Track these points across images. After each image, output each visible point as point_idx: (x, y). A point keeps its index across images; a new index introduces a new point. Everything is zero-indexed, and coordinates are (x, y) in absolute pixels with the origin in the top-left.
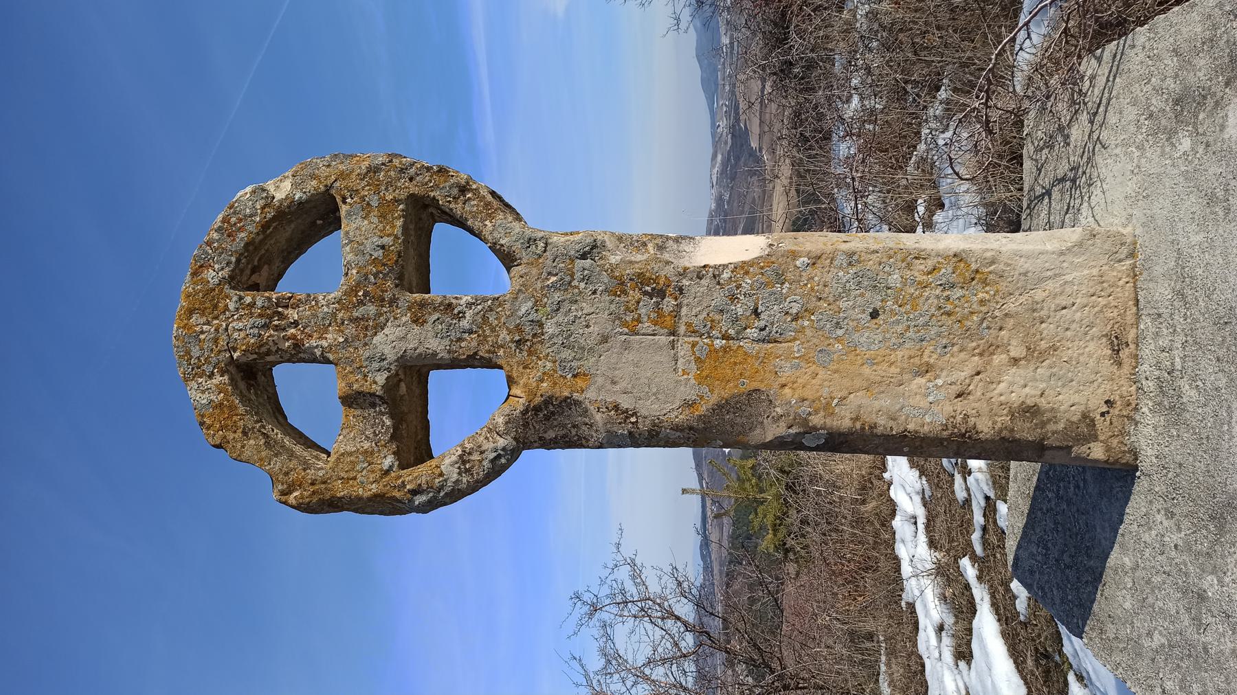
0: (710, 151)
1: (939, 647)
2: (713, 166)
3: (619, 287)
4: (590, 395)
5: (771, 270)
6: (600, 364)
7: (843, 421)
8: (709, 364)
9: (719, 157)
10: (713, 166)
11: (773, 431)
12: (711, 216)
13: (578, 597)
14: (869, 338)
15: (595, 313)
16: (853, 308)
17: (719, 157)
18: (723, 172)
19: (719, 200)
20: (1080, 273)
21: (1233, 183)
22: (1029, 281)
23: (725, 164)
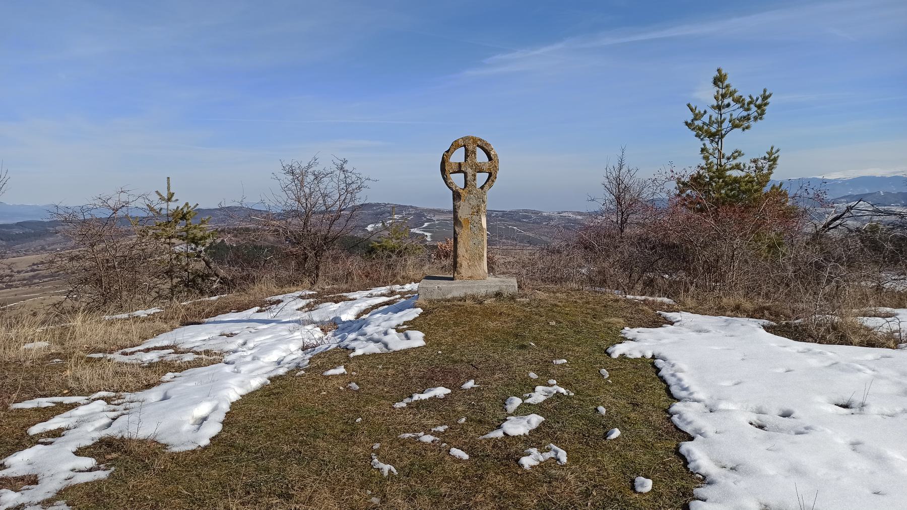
0: (584, 211)
1: (292, 322)
2: (574, 213)
3: (478, 206)
4: (461, 202)
5: (481, 229)
6: (466, 203)
7: (459, 240)
8: (467, 220)
9: (580, 217)
10: (574, 213)
11: (457, 229)
12: (536, 213)
13: (345, 162)
14: (471, 243)
15: (474, 202)
16: (475, 241)
17: (580, 217)
18: (569, 220)
19: (550, 218)
20: (481, 272)
21: (530, 501)
22: (480, 265)
23: (575, 221)
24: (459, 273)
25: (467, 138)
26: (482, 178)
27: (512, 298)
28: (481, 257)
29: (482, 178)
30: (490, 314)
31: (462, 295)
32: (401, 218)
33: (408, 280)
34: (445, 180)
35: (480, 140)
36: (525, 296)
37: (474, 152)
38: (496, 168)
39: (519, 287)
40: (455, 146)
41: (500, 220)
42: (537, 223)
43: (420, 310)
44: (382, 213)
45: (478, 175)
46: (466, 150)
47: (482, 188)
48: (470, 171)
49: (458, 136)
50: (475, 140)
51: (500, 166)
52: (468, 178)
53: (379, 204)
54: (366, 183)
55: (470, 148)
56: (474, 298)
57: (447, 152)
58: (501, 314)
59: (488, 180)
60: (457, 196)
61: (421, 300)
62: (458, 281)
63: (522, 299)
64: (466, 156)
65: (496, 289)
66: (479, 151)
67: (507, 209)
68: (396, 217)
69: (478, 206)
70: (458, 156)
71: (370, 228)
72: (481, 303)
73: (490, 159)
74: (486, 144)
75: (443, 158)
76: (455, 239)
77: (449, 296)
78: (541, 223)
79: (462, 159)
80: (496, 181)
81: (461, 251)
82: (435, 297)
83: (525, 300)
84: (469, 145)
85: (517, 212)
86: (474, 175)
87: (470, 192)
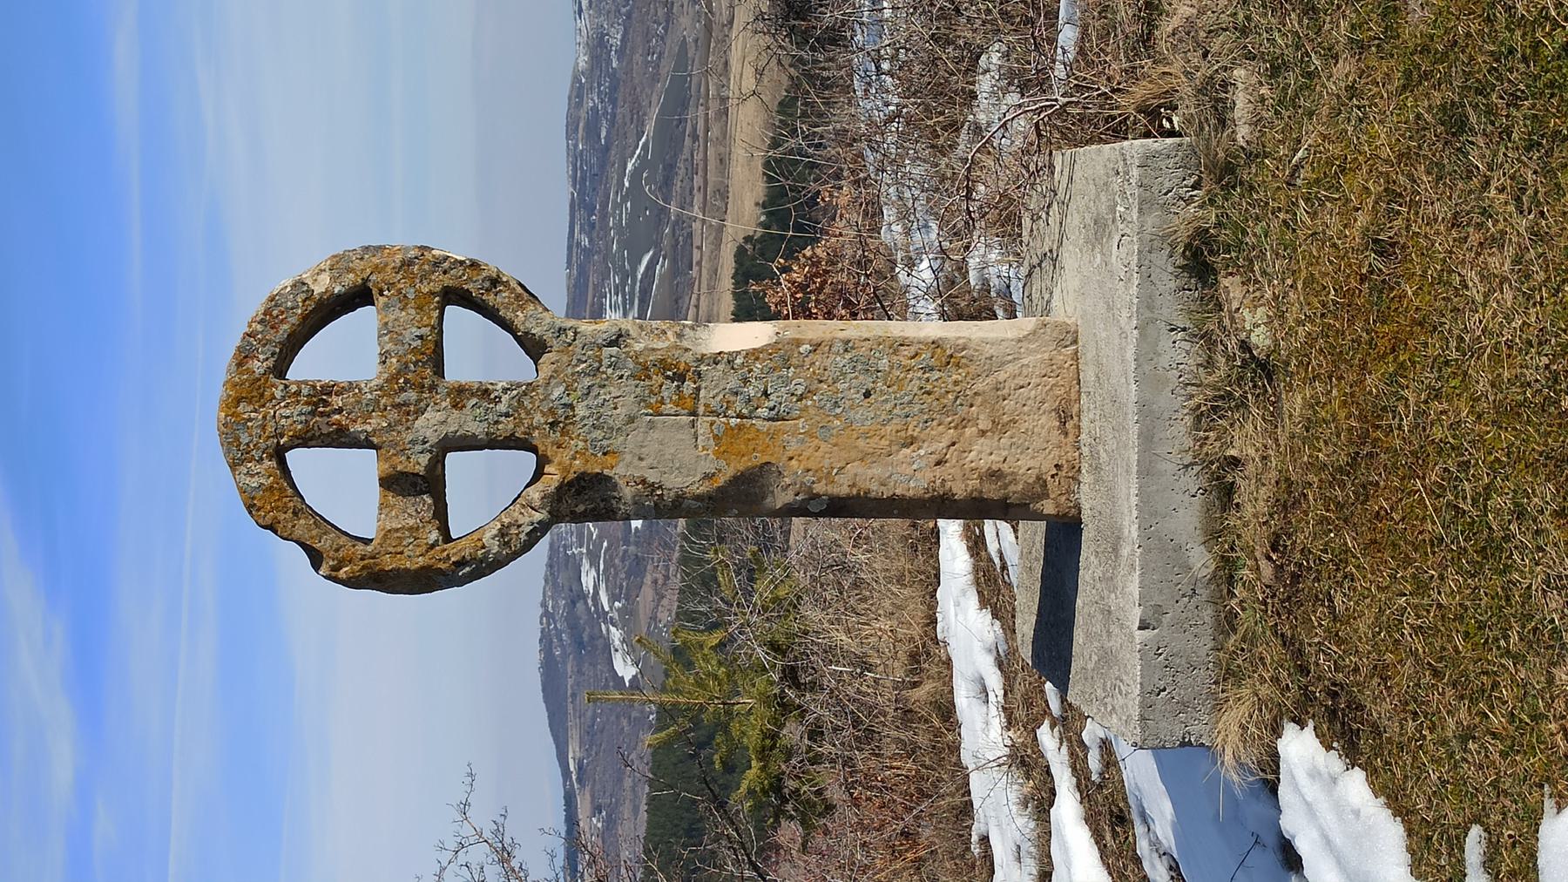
3: (643, 373)
5: (779, 356)
6: (628, 443)
7: (842, 489)
8: (725, 441)
11: (782, 498)
12: (578, 94)
14: (862, 414)
15: (623, 396)
19: (598, 46)
20: (1034, 359)
22: (994, 364)
24: (1040, 488)
25: (231, 432)
26: (474, 349)
27: (1225, 174)
28: (947, 357)
29: (474, 349)
30: (1376, 310)
31: (1192, 481)
32: (594, 563)
33: (927, 654)
34: (481, 566)
35: (243, 356)
36: (1215, 96)
37: (321, 395)
38: (417, 263)
39: (1153, 120)
40: (279, 508)
41: (604, 217)
42: (614, 88)
43: (1299, 748)
44: (574, 626)
45: (458, 369)
46: (305, 439)
47: (534, 347)
48: (432, 423)
49: (214, 488)
50: (247, 392)
51: (401, 236)
52: (477, 429)
53: (546, 641)
54: (482, 818)
55: (291, 416)
56: (1213, 412)
57: (316, 559)
58: (1384, 249)
59: (490, 313)
60: (584, 498)
61: (1228, 730)
62: (1088, 499)
63: (1241, 104)
64: (341, 438)
65: (1167, 282)
66: (310, 365)
67: (561, 192)
68: (588, 581)
69: (643, 373)
70: (342, 485)
71: (625, 669)
72: (1262, 369)
73: (359, 297)
74: (269, 317)
75: (353, 583)
76: (838, 507)
77: (1201, 561)
78: (613, 75)
79: (363, 466)
80: (494, 262)
81: (910, 474)
82: (1203, 645)
83: (1246, 90)
84: (273, 420)
85: (575, 158)
86: (460, 394)
87: (560, 423)
